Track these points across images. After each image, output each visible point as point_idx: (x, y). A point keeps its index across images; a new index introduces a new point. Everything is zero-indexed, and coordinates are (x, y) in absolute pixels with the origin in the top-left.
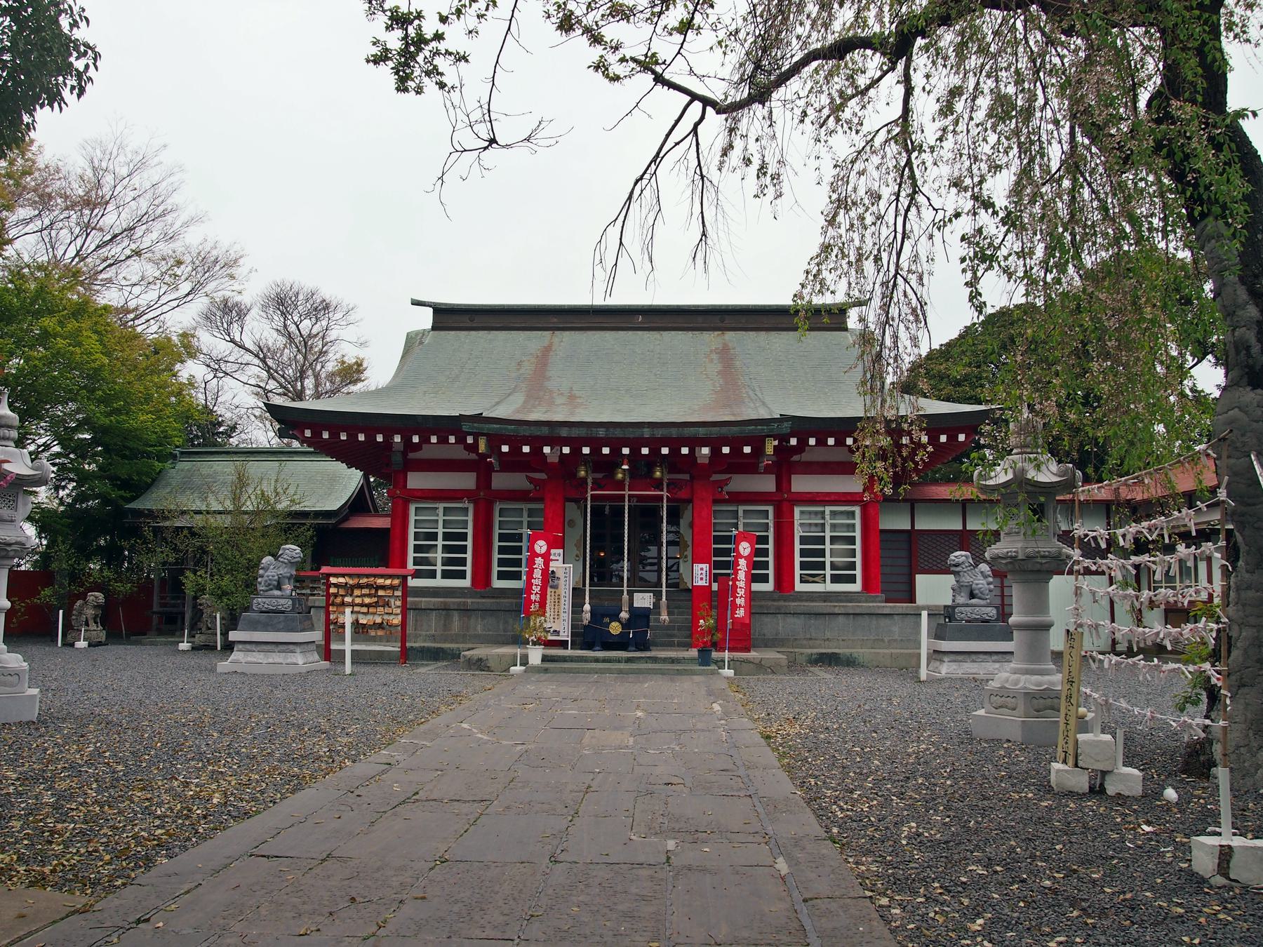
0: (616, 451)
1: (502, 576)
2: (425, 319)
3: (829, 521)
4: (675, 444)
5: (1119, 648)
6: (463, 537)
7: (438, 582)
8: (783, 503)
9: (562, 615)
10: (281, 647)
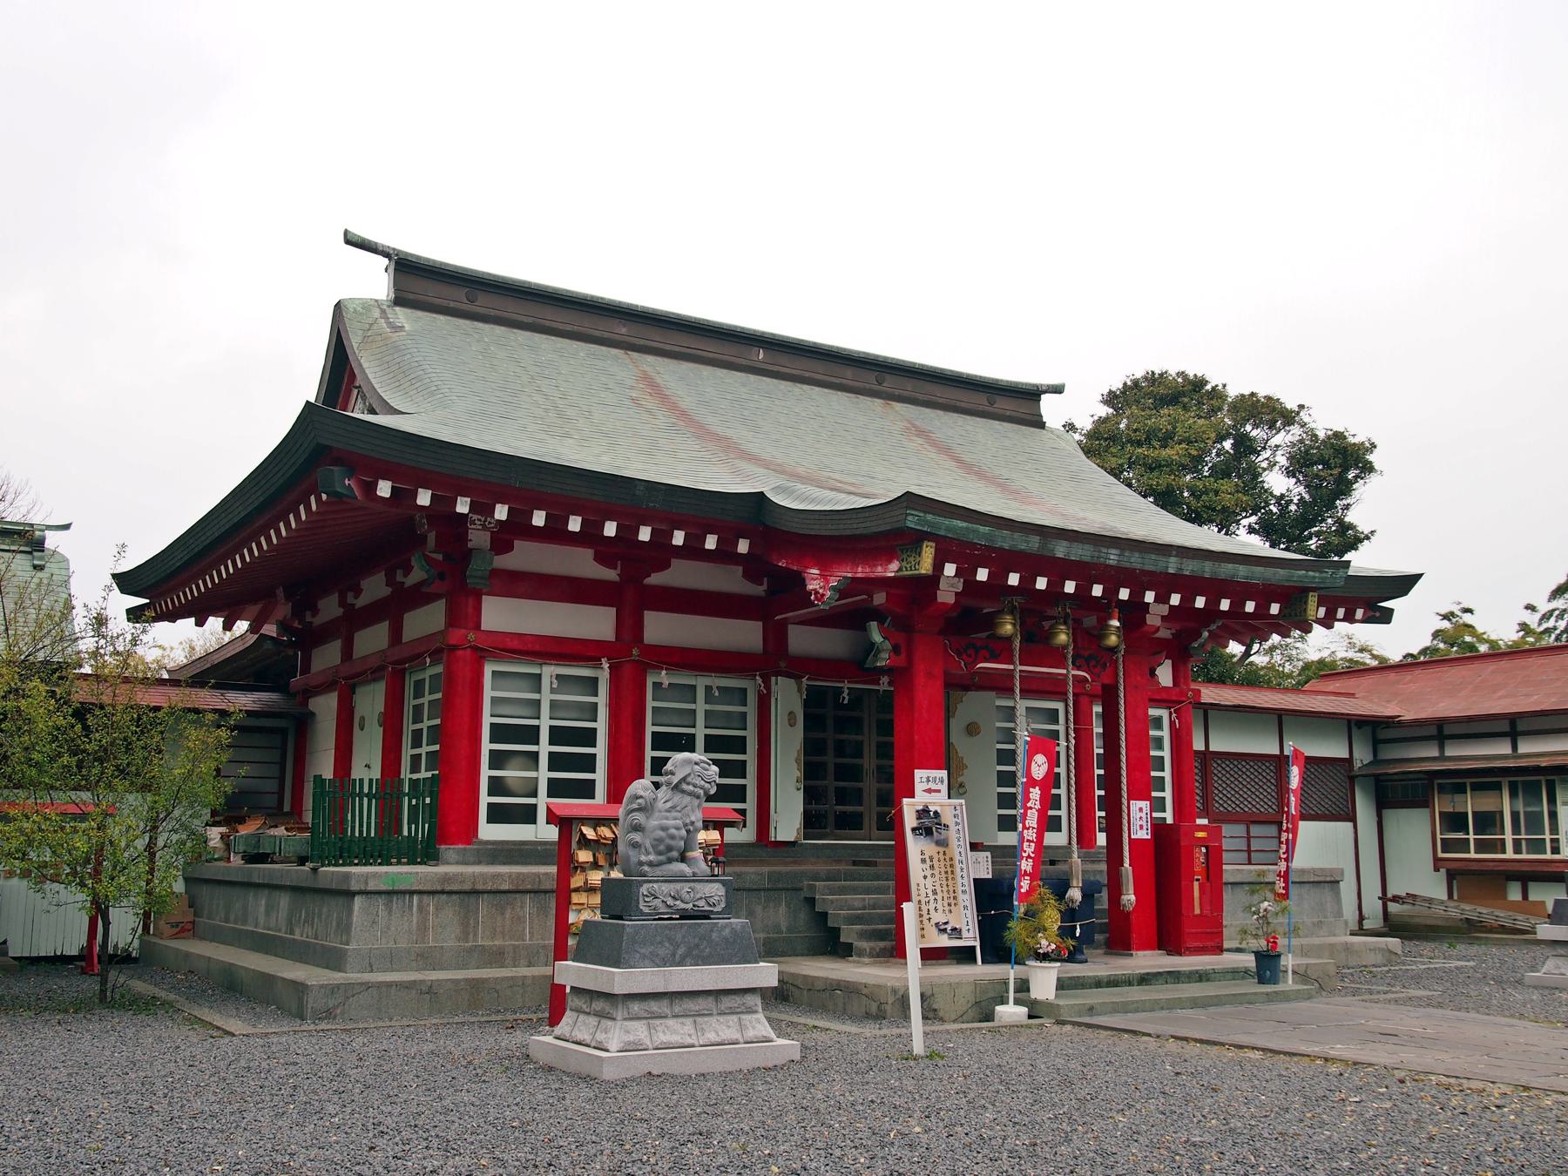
1: (499, 815)
2: (372, 281)
5: (1367, 925)
6: (589, 737)
9: (961, 897)
10: (727, 1002)
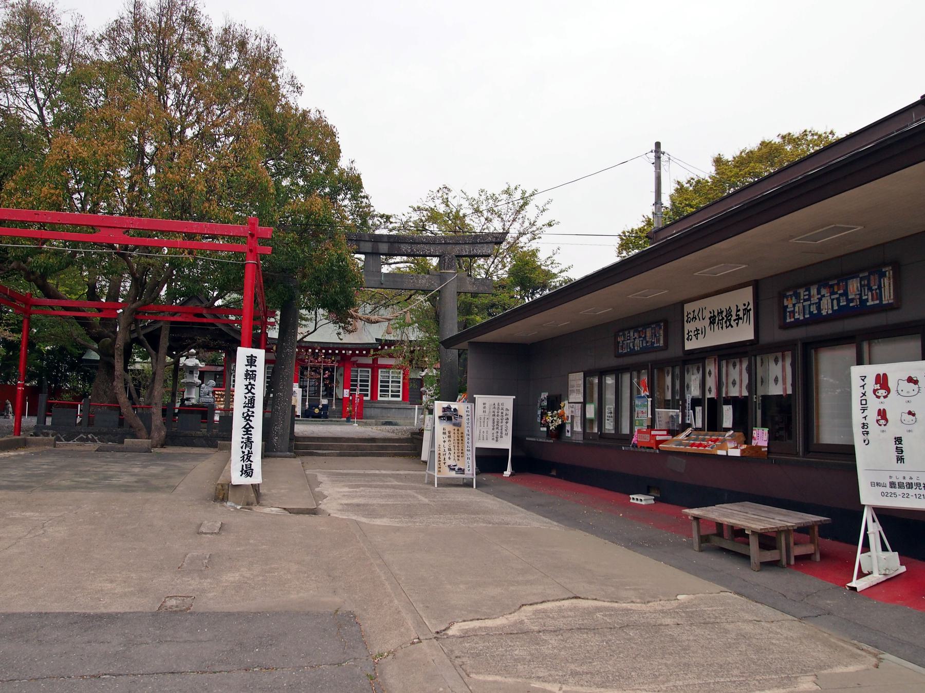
0: (320, 350)
3: (391, 375)
4: (340, 350)
6: (367, 381)
7: (391, 399)
8: (375, 367)
